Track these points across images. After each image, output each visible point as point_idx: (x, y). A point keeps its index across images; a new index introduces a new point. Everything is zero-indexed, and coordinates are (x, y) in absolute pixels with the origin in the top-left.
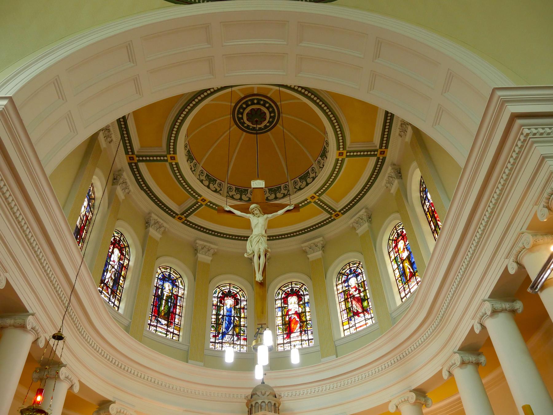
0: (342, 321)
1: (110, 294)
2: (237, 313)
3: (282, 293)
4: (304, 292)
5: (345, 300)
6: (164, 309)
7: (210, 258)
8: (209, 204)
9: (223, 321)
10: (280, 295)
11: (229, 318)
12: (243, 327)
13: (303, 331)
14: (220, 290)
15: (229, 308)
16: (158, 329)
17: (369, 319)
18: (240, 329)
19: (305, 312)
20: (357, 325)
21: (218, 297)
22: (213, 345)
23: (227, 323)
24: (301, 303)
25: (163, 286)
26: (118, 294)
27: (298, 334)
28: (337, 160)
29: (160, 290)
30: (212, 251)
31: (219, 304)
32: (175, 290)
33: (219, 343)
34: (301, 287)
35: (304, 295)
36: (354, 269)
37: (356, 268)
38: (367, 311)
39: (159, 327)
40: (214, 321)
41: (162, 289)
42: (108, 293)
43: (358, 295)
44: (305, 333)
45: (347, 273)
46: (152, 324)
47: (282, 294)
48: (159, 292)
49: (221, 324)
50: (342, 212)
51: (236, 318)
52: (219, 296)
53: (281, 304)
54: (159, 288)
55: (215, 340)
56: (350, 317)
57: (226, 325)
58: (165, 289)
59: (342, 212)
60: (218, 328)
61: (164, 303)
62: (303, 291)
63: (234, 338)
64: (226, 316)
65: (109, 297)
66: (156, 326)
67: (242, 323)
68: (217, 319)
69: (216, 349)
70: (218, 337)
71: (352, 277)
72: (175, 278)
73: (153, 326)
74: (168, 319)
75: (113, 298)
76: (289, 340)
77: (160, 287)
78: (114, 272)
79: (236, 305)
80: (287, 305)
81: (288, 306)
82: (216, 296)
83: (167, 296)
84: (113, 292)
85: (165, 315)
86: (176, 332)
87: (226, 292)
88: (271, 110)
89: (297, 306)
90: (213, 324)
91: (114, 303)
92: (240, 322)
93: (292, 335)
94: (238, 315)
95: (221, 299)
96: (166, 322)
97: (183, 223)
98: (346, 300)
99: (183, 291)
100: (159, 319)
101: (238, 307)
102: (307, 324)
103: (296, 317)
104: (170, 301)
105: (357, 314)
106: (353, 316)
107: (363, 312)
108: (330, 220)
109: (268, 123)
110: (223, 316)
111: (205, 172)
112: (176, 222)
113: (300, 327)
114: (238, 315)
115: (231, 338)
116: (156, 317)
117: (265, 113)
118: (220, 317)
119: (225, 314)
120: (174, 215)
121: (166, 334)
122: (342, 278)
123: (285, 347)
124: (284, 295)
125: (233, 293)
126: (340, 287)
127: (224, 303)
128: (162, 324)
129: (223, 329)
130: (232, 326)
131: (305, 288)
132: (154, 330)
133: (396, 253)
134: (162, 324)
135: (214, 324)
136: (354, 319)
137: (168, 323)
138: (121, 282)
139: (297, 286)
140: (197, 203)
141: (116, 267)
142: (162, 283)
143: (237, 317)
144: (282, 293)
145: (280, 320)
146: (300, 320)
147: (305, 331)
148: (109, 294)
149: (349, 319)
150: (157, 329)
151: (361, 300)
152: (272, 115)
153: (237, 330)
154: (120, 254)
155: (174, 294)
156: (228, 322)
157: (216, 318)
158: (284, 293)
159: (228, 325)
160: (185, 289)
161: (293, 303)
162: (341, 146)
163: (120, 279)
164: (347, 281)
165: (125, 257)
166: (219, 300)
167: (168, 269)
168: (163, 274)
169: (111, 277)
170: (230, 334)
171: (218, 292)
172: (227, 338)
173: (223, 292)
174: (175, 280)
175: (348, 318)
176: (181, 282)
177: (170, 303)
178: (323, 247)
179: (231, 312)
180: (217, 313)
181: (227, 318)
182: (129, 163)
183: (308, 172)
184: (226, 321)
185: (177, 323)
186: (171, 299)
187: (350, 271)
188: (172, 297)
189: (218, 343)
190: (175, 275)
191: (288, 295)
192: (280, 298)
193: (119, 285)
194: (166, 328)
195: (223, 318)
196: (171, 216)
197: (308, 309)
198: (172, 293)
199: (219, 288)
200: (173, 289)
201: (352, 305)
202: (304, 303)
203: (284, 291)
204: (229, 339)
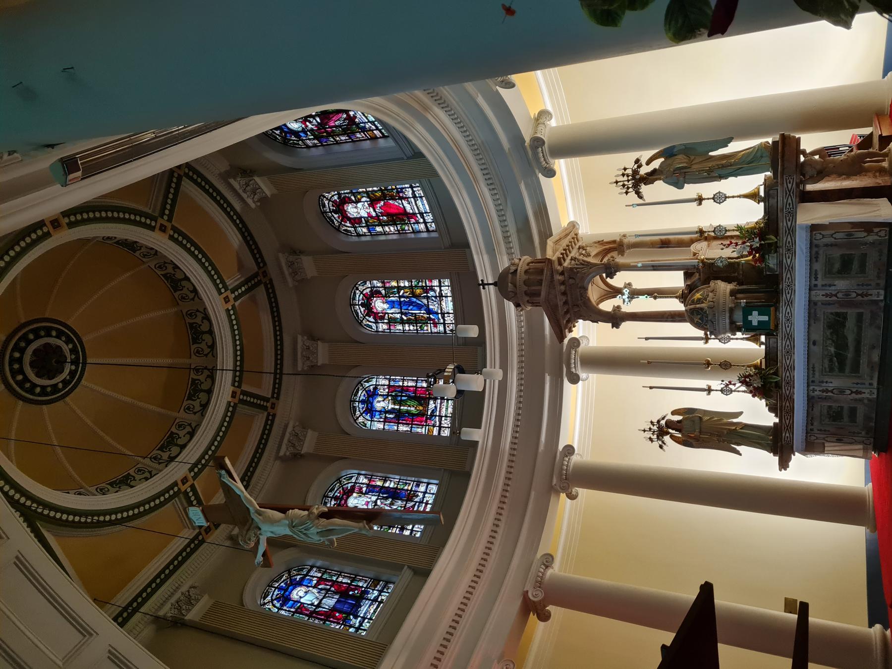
0: (368, 139)
1: (413, 503)
2: (393, 293)
6: (413, 407)
9: (409, 313)
10: (349, 229)
14: (363, 319)
15: (388, 306)
16: (443, 413)
18: (416, 286)
22: (448, 327)
23: (411, 307)
24: (353, 198)
25: (380, 411)
26: (410, 488)
29: (387, 415)
31: (386, 321)
32: (381, 390)
33: (443, 318)
39: (440, 411)
40: (414, 326)
41: (386, 412)
46: (438, 424)
47: (347, 226)
48: (391, 416)
49: (415, 316)
54: (386, 417)
55: (441, 323)
56: (359, 128)
57: (414, 308)
58: (384, 408)
60: (421, 320)
61: (406, 408)
63: (432, 296)
65: (417, 504)
66: (440, 417)
68: (409, 322)
69: (453, 322)
70: (434, 319)
72: (364, 392)
73: (440, 423)
75: (418, 496)
77: (383, 416)
78: (382, 501)
79: (381, 294)
80: (363, 219)
81: (364, 218)
82: (374, 325)
83: (394, 404)
85: (421, 405)
87: (364, 311)
88: (23, 344)
89: (360, 205)
90: (418, 328)
91: (425, 493)
92: (405, 287)
93: (408, 209)
94: (396, 290)
95: (379, 317)
96: (431, 402)
97: (278, 398)
100: (429, 414)
101: (384, 291)
103: (378, 205)
106: (355, 123)
108: (191, 174)
109: (51, 336)
110: (402, 313)
111: (185, 403)
112: (279, 411)
113: (393, 199)
114: (396, 290)
115: (433, 300)
116: (427, 419)
117: (35, 352)
118: (405, 318)
119: (398, 310)
125: (363, 299)
127: (382, 313)
128: (436, 407)
129: (422, 313)
130: (414, 300)
132: (446, 420)
134: (436, 407)
135: (417, 326)
136: (361, 123)
138: (392, 485)
141: (374, 498)
143: (399, 293)
144: (344, 225)
145: (389, 228)
146: (382, 200)
147: (398, 192)
148: (415, 505)
149: (364, 130)
150: (444, 415)
152: (31, 336)
153: (418, 291)
154: (355, 495)
155: (388, 392)
157: (408, 323)
159: (414, 306)
161: (355, 210)
162: (39, 232)
163: (389, 487)
165: (355, 483)
167: (354, 405)
170: (428, 302)
171: (368, 323)
172: (434, 307)
174: (366, 392)
176: (367, 382)
177: (404, 398)
179: (393, 302)
180: (400, 323)
181: (404, 307)
182: (216, 529)
184: (409, 308)
186: (396, 396)
188: (393, 394)
189: (444, 320)
191: (345, 217)
192: (353, 229)
194: (439, 401)
195: (406, 314)
196: (273, 421)
198: (388, 396)
200: (381, 395)
202: (353, 194)
203: (341, 223)
204: (435, 303)
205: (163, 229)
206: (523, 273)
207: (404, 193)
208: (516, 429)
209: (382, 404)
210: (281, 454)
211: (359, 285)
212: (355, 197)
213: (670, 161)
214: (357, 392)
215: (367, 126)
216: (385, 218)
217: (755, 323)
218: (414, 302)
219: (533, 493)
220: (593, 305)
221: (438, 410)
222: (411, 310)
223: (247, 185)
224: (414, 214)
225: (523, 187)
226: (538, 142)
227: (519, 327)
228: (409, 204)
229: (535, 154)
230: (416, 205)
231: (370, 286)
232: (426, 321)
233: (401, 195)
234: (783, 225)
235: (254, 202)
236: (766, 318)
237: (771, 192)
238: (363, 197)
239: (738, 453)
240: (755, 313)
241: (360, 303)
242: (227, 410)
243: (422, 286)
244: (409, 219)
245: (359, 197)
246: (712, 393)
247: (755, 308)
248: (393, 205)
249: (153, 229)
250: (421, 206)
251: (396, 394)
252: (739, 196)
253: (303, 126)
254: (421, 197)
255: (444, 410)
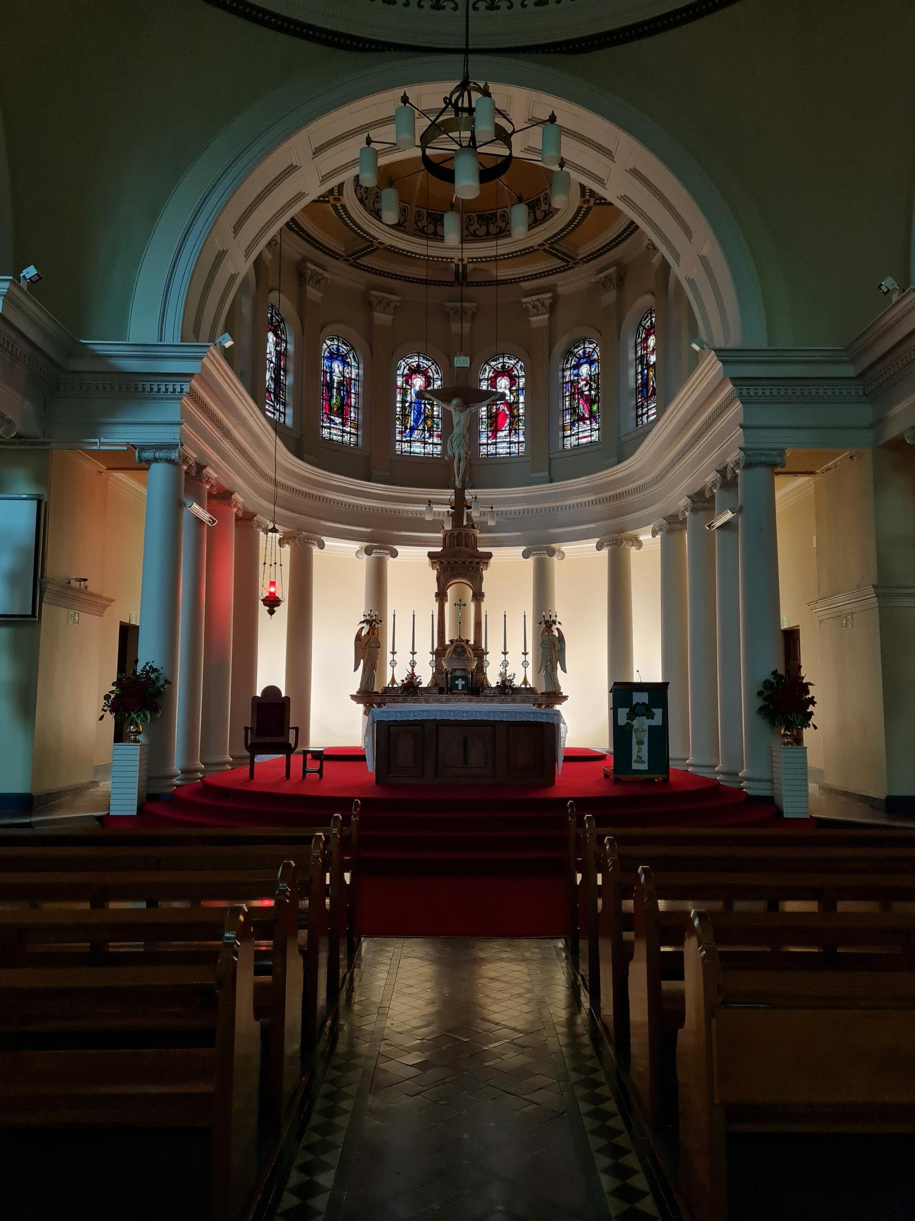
0: (564, 424)
1: (273, 399)
3: (490, 370)
4: (520, 371)
5: (570, 395)
7: (391, 317)
8: (389, 247)
10: (487, 373)
11: (418, 407)
12: (437, 418)
13: (513, 430)
17: (596, 430)
18: (433, 421)
19: (518, 403)
20: (581, 435)
21: (403, 376)
23: (416, 413)
24: (514, 388)
25: (331, 367)
27: (506, 433)
28: (580, 208)
29: (328, 374)
30: (392, 305)
31: (404, 385)
33: (406, 441)
34: (516, 364)
35: (519, 377)
36: (590, 352)
37: (591, 350)
38: (594, 418)
40: (400, 412)
41: (331, 373)
42: (271, 401)
43: (587, 393)
44: (516, 433)
45: (579, 355)
46: (325, 425)
48: (328, 378)
49: (408, 415)
50: (585, 260)
51: (427, 406)
52: (405, 373)
53: (488, 387)
54: (327, 372)
56: (574, 421)
57: (415, 416)
58: (334, 372)
59: (585, 260)
60: (405, 420)
61: (335, 394)
62: (517, 370)
64: (414, 403)
66: (330, 428)
67: (435, 413)
68: (403, 408)
71: (585, 363)
72: (346, 352)
74: (343, 415)
76: (494, 441)
77: (328, 370)
82: (401, 373)
83: (338, 383)
84: (277, 396)
86: (353, 431)
87: (413, 366)
92: (433, 411)
93: (500, 434)
95: (408, 378)
96: (340, 420)
97: (351, 265)
98: (572, 395)
99: (357, 371)
102: (519, 419)
103: (506, 409)
104: (342, 388)
105: (582, 419)
106: (578, 421)
107: (589, 419)
110: (411, 403)
113: (511, 424)
116: (328, 414)
118: (407, 405)
120: (338, 256)
121: (343, 436)
122: (572, 360)
123: (489, 449)
124: (493, 373)
125: (424, 367)
126: (567, 373)
128: (336, 424)
129: (411, 423)
130: (422, 417)
131: (521, 365)
133: (644, 350)
134: (336, 424)
137: (343, 420)
139: (510, 362)
140: (372, 246)
142: (330, 364)
145: (484, 411)
146: (510, 413)
147: (515, 430)
149: (572, 424)
151: (590, 401)
154: (275, 338)
155: (346, 377)
156: (417, 412)
157: (402, 406)
158: (493, 370)
159: (417, 416)
160: (360, 366)
161: (503, 386)
164: (577, 366)
166: (404, 379)
168: (330, 349)
169: (271, 377)
170: (420, 430)
173: (409, 367)
175: (571, 422)
176: (354, 357)
177: (342, 392)
178: (551, 305)
180: (402, 399)
183: (539, 199)
185: (353, 419)
186: (344, 385)
187: (584, 352)
189: (405, 442)
190: (345, 347)
193: (281, 383)
195: (410, 406)
196: (334, 257)
197: (522, 399)
198: (343, 376)
199: (404, 361)
201: (579, 405)
202: (518, 390)
203: (492, 368)
205: (542, 245)
206: (473, 533)
207: (515, 435)
208: (336, 502)
209: (337, 370)
210: (309, 265)
211: (436, 367)
212: (515, 390)
213: (557, 640)
214: (346, 345)
215: (575, 428)
216: (494, 411)
217: (457, 682)
218: (420, 417)
219: (297, 515)
220: (93, 428)
221: (335, 426)
222: (414, 413)
223: (543, 305)
224: (495, 437)
225: (518, 534)
226: (552, 552)
227: (407, 512)
228: (505, 436)
229: (543, 549)
230: (504, 442)
231: (435, 377)
232: (404, 424)
233: (513, 431)
234: (518, 697)
235: (527, 303)
236: (460, 688)
237: (530, 691)
238: (514, 397)
239: (356, 669)
240: (464, 682)
241: (420, 363)
242: (528, 249)
243: (433, 428)
244: (492, 431)
245: (515, 394)
246: (412, 655)
247: (467, 683)
248: (505, 422)
249: (546, 241)
250: (502, 445)
251: (345, 384)
252: (525, 675)
253: (583, 378)
254: (510, 448)
255: (335, 432)
